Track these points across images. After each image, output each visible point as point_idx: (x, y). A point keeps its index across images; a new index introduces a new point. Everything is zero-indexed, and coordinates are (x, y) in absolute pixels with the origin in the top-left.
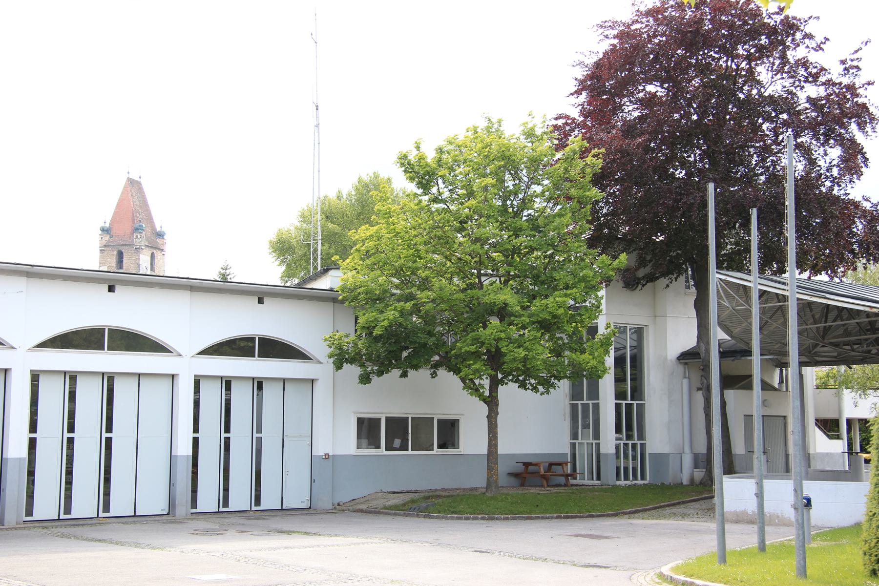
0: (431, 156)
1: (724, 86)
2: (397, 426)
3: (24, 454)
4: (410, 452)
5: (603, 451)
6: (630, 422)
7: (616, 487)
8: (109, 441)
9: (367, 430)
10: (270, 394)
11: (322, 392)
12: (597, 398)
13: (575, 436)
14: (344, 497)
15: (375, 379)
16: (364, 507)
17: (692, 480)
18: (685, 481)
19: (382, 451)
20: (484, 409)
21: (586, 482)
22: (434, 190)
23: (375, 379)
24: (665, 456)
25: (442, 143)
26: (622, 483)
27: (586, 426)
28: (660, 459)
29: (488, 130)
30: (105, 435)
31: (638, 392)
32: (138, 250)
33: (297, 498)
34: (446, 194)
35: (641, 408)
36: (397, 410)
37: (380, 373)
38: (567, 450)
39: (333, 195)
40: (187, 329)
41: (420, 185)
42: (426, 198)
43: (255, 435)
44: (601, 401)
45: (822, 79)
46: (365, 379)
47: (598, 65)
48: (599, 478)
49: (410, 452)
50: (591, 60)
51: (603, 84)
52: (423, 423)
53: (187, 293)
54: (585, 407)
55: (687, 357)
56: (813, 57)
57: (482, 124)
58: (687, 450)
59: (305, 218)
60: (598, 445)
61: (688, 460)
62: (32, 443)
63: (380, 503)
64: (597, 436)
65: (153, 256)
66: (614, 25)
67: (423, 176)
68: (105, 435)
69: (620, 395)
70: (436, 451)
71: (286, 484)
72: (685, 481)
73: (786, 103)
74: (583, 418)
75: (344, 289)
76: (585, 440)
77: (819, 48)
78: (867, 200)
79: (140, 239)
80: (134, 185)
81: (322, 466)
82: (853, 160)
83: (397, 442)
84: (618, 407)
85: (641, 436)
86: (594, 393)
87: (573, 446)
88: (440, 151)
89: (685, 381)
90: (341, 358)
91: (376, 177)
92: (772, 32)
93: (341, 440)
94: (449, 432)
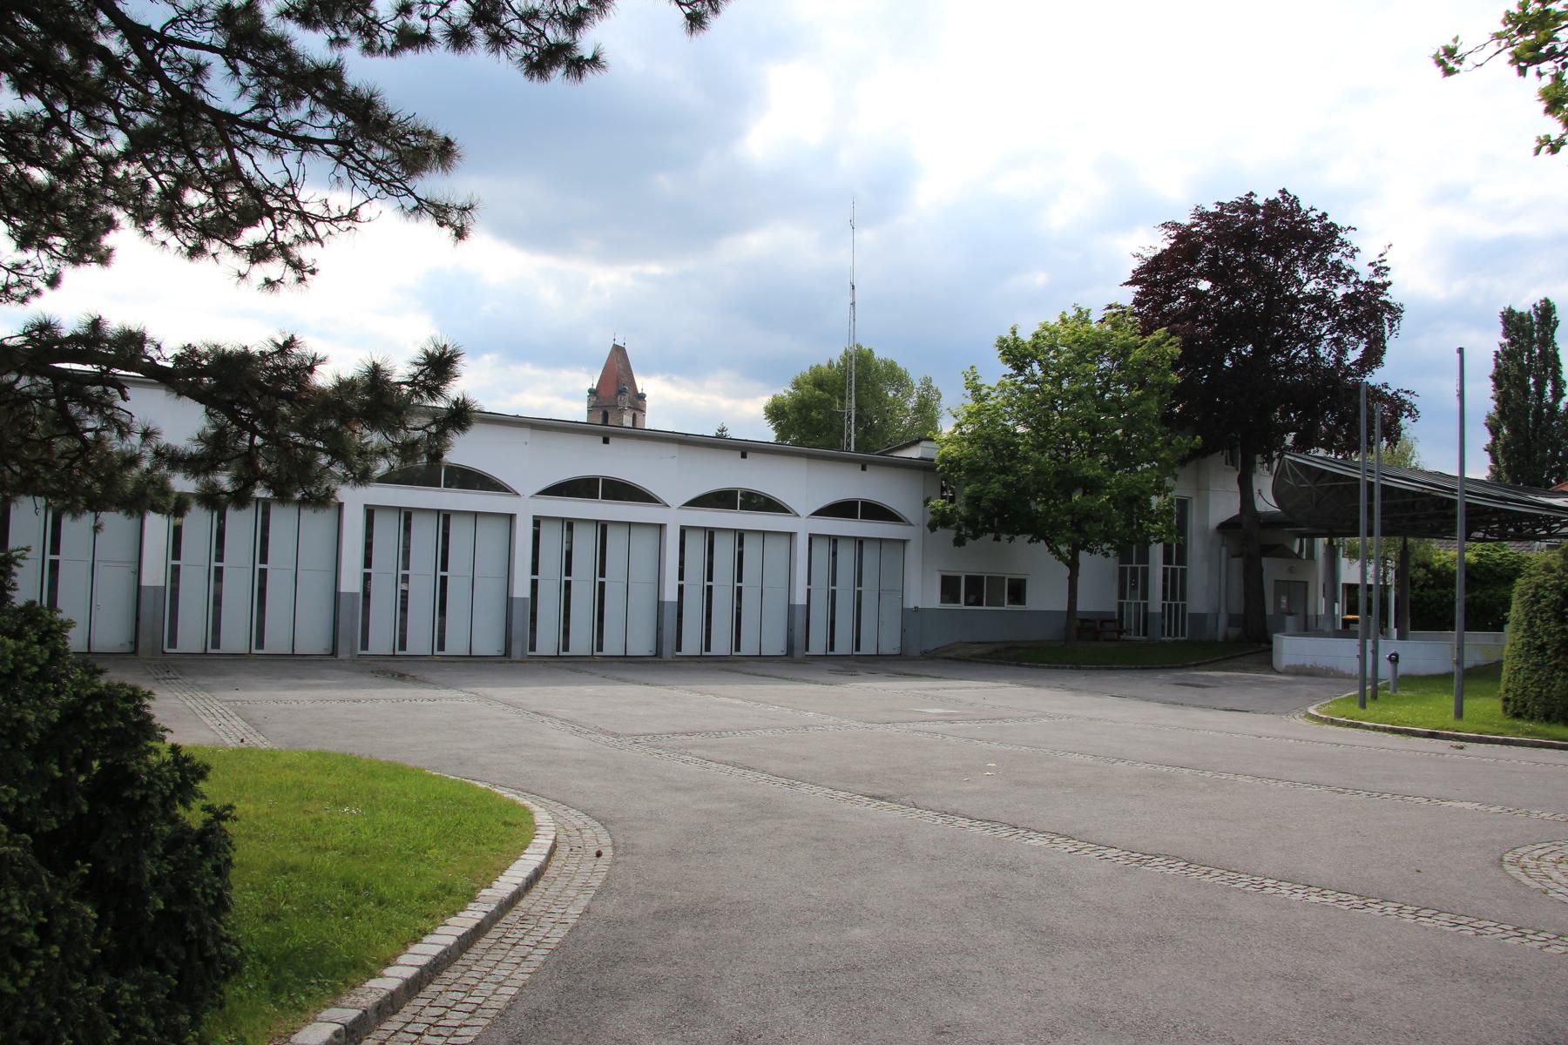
0: (1026, 336)
1: (1273, 285)
2: (974, 583)
3: (527, 594)
4: (984, 608)
5: (1150, 610)
6: (1175, 585)
7: (1162, 642)
8: (444, 580)
9: (949, 587)
10: (870, 555)
11: (913, 554)
12: (1147, 562)
13: (1122, 595)
14: (930, 646)
15: (969, 542)
16: (952, 655)
17: (1226, 635)
18: (1220, 638)
19: (962, 606)
20: (1067, 571)
21: (1133, 637)
22: (1027, 371)
23: (969, 542)
24: (1205, 616)
25: (1037, 329)
26: (1166, 638)
27: (1134, 588)
28: (1199, 619)
29: (1078, 317)
30: (440, 573)
31: (1182, 559)
32: (622, 411)
33: (891, 645)
34: (1039, 373)
35: (1184, 572)
36: (974, 569)
37: (975, 537)
38: (1115, 609)
39: (824, 364)
40: (674, 482)
41: (1015, 367)
42: (1021, 378)
43: (49, 557)
44: (1150, 566)
45: (1353, 279)
46: (959, 542)
47: (1157, 259)
48: (1145, 634)
49: (984, 608)
50: (1150, 255)
51: (1157, 276)
52: (996, 581)
53: (805, 460)
54: (1134, 570)
55: (1226, 527)
56: (1346, 262)
57: (1071, 313)
58: (1223, 610)
59: (797, 385)
60: (1146, 605)
61: (1223, 620)
62: (534, 584)
63: (977, 651)
64: (1145, 596)
65: (634, 417)
66: (1176, 226)
67: (1015, 354)
68: (440, 573)
69: (1167, 558)
70: (1007, 607)
71: (883, 635)
72: (1220, 638)
73: (1320, 299)
74: (1131, 581)
75: (943, 459)
76: (1132, 601)
77: (1352, 256)
78: (158, 347)
79: (624, 401)
80: (619, 352)
81: (912, 617)
82: (1373, 357)
83: (972, 598)
84: (1165, 570)
85: (1183, 598)
86: (1144, 557)
87: (1121, 605)
88: (1036, 336)
89: (1224, 550)
90: (940, 521)
91: (96, 324)
92: (1318, 239)
93: (923, 592)
94: (1017, 591)
